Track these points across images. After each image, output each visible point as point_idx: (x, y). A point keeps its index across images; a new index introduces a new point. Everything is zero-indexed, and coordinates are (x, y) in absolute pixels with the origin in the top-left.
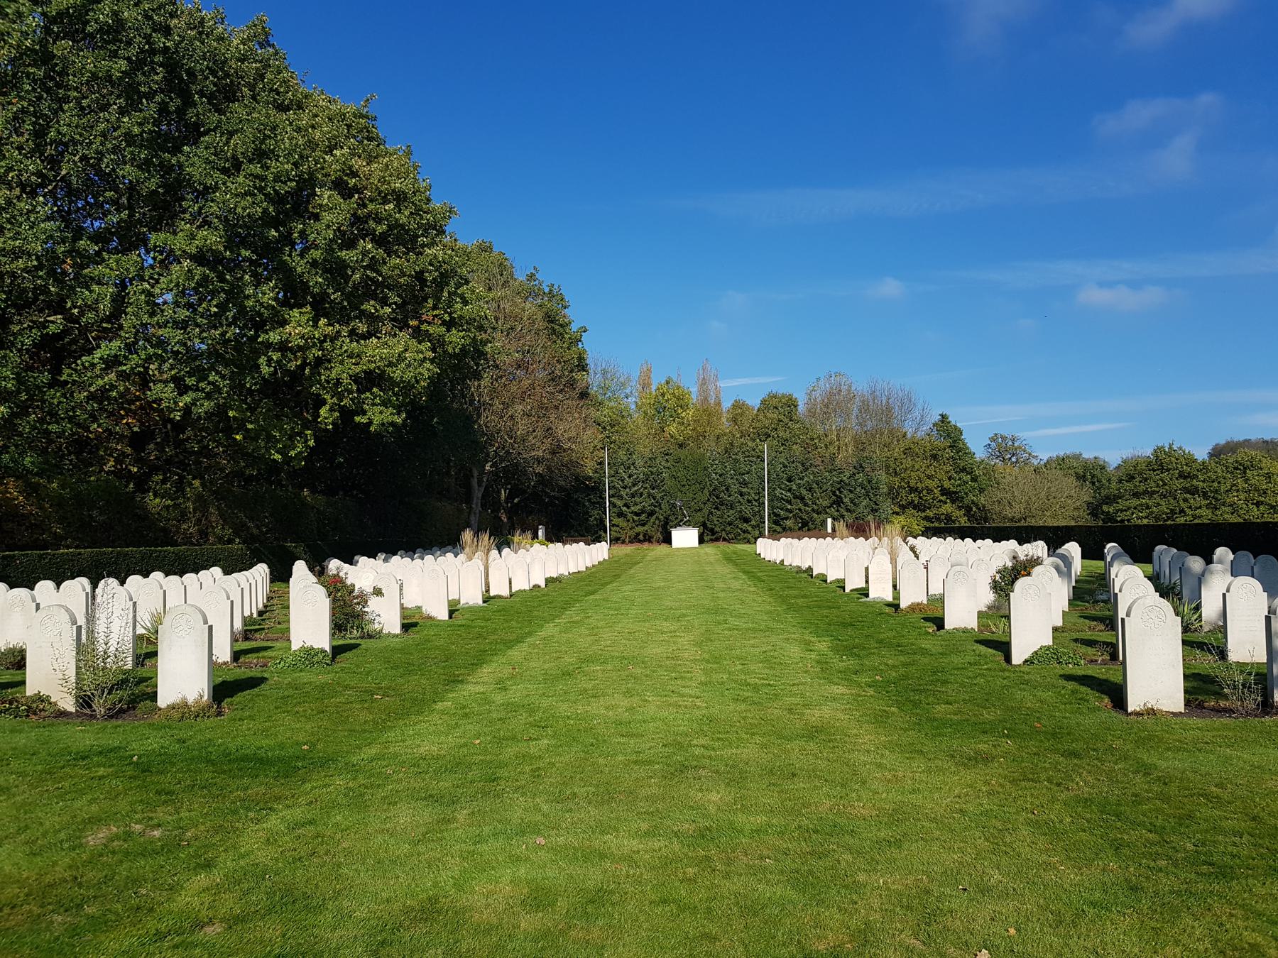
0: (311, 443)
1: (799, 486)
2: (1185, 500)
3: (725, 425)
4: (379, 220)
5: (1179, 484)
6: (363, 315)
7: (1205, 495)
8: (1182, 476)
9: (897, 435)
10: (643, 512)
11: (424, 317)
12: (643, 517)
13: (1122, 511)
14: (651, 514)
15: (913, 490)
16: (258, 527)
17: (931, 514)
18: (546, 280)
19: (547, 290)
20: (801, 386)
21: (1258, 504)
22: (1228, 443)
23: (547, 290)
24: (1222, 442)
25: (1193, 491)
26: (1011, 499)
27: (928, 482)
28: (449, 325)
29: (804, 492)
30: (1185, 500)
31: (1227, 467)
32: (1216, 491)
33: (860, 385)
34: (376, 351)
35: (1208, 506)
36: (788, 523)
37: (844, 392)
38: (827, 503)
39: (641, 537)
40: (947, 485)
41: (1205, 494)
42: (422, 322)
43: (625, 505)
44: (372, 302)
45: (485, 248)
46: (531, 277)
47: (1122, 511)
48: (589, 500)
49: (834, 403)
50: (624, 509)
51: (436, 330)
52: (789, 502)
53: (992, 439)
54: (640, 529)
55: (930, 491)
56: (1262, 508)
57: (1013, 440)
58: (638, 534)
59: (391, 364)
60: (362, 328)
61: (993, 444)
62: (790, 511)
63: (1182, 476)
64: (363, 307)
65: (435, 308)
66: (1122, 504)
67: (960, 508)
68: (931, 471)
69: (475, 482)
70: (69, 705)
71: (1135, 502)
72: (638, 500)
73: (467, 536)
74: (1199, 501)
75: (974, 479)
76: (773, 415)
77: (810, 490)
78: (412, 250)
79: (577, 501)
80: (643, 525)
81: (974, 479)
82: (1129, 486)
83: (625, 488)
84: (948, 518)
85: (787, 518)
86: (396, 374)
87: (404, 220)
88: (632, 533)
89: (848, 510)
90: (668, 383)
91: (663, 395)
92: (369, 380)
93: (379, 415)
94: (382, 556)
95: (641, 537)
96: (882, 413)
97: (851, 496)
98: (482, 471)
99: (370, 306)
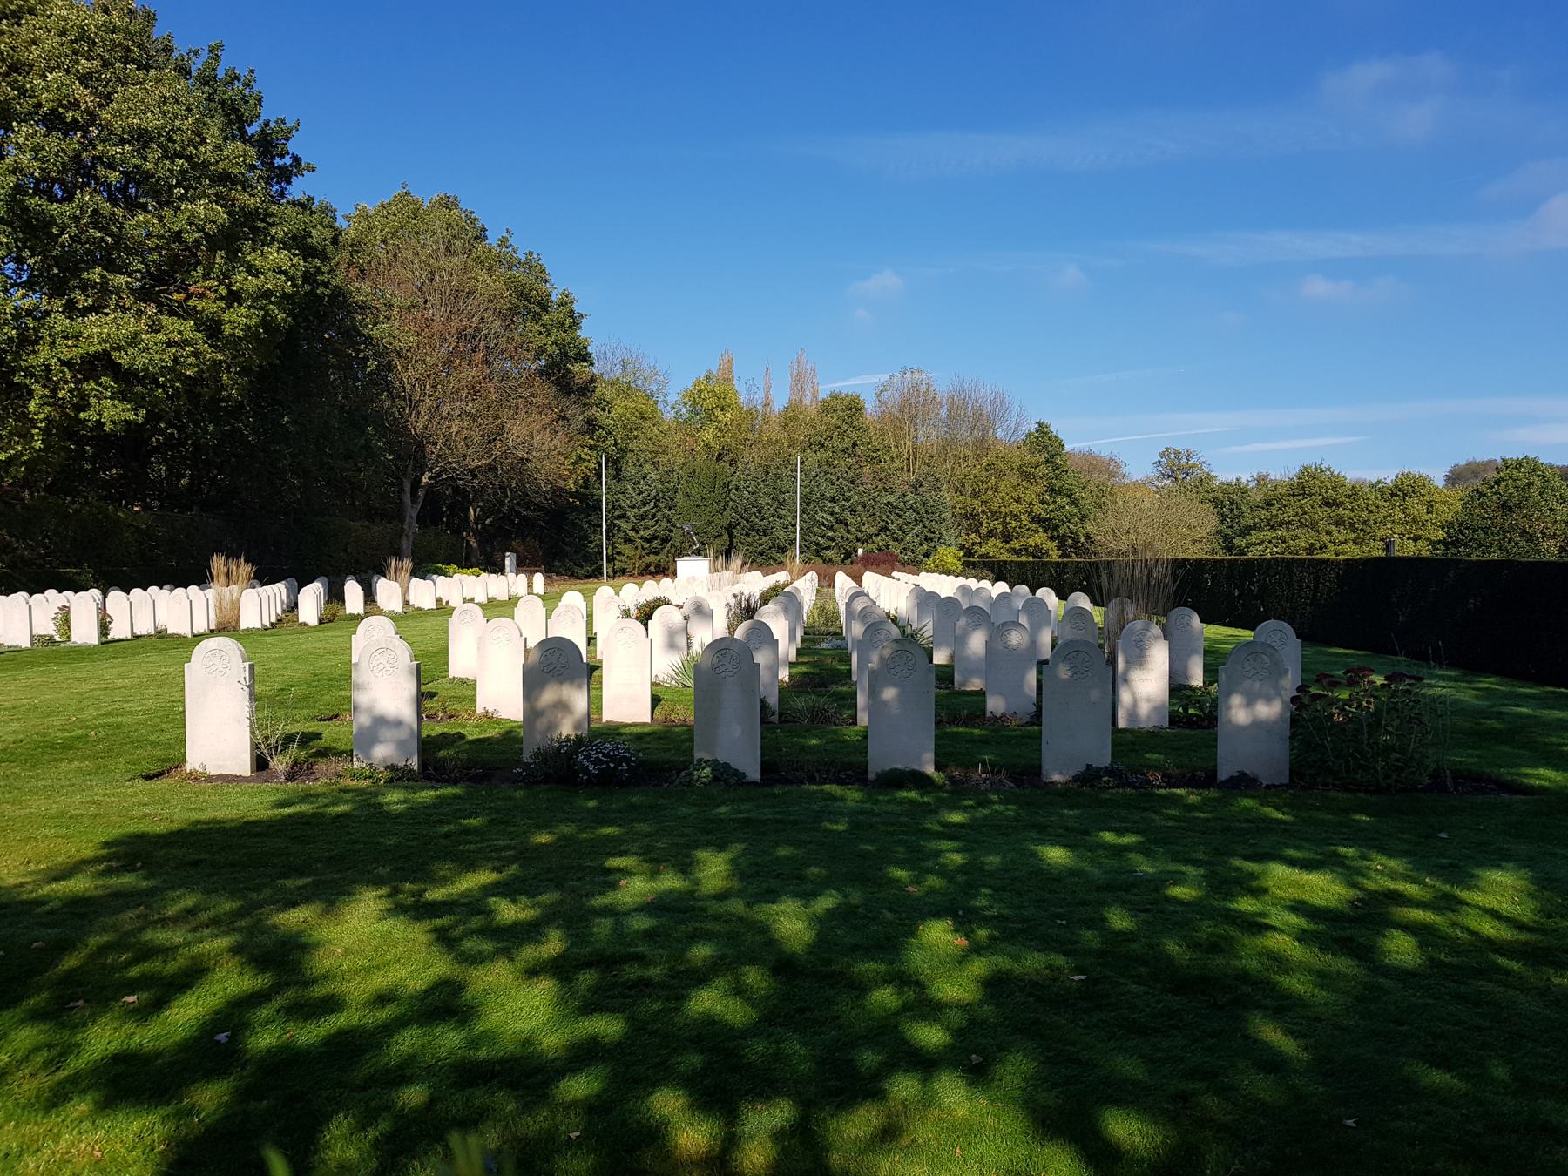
0: (38, 445)
1: (843, 509)
2: (1329, 533)
3: (774, 431)
4: (111, 166)
5: (1321, 513)
6: (85, 287)
7: (1353, 529)
8: (1327, 503)
9: (982, 446)
10: (656, 538)
11: (191, 289)
12: (656, 544)
13: (1254, 544)
14: (665, 540)
15: (995, 515)
16: (32, 549)
17: (1017, 546)
18: (522, 248)
19: (523, 259)
20: (868, 383)
21: (1416, 539)
22: (1469, 464)
23: (523, 259)
24: (1463, 463)
25: (1339, 522)
26: (1111, 534)
27: (1015, 507)
28: (233, 298)
29: (847, 516)
30: (1329, 533)
31: (1383, 493)
32: (1365, 522)
33: (942, 381)
34: (97, 331)
35: (1355, 541)
36: (829, 554)
37: (923, 388)
38: (874, 530)
39: (652, 569)
40: (1037, 510)
41: (1352, 525)
42: (189, 297)
43: (633, 529)
44: (98, 270)
45: (447, 204)
46: (503, 242)
47: (1254, 544)
48: (589, 522)
49: (911, 407)
50: (632, 533)
51: (208, 306)
52: (831, 528)
53: (1163, 455)
54: (652, 558)
55: (1016, 517)
56: (1419, 543)
57: (1188, 458)
58: (648, 565)
59: (119, 348)
60: (83, 301)
61: (1164, 460)
62: (832, 539)
63: (1327, 503)
64: (85, 275)
65: (206, 277)
66: (1255, 536)
67: (1052, 538)
68: (1021, 492)
69: (407, 498)
70: (754, 773)
71: (1270, 534)
72: (651, 523)
73: (218, 563)
74: (1346, 534)
75: (1075, 503)
76: (832, 420)
77: (853, 511)
78: (169, 203)
79: (574, 524)
80: (657, 553)
81: (1075, 503)
82: (1264, 514)
83: (633, 507)
84: (1038, 552)
85: (828, 548)
86: (122, 358)
87: (148, 166)
88: (641, 564)
89: (895, 539)
90: (707, 378)
91: (700, 391)
92: (98, 365)
93: (109, 411)
94: (167, 587)
95: (652, 569)
96: (972, 417)
97: (900, 521)
98: (416, 483)
99: (95, 275)
